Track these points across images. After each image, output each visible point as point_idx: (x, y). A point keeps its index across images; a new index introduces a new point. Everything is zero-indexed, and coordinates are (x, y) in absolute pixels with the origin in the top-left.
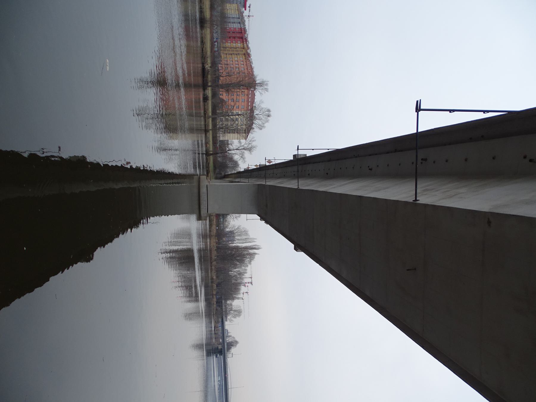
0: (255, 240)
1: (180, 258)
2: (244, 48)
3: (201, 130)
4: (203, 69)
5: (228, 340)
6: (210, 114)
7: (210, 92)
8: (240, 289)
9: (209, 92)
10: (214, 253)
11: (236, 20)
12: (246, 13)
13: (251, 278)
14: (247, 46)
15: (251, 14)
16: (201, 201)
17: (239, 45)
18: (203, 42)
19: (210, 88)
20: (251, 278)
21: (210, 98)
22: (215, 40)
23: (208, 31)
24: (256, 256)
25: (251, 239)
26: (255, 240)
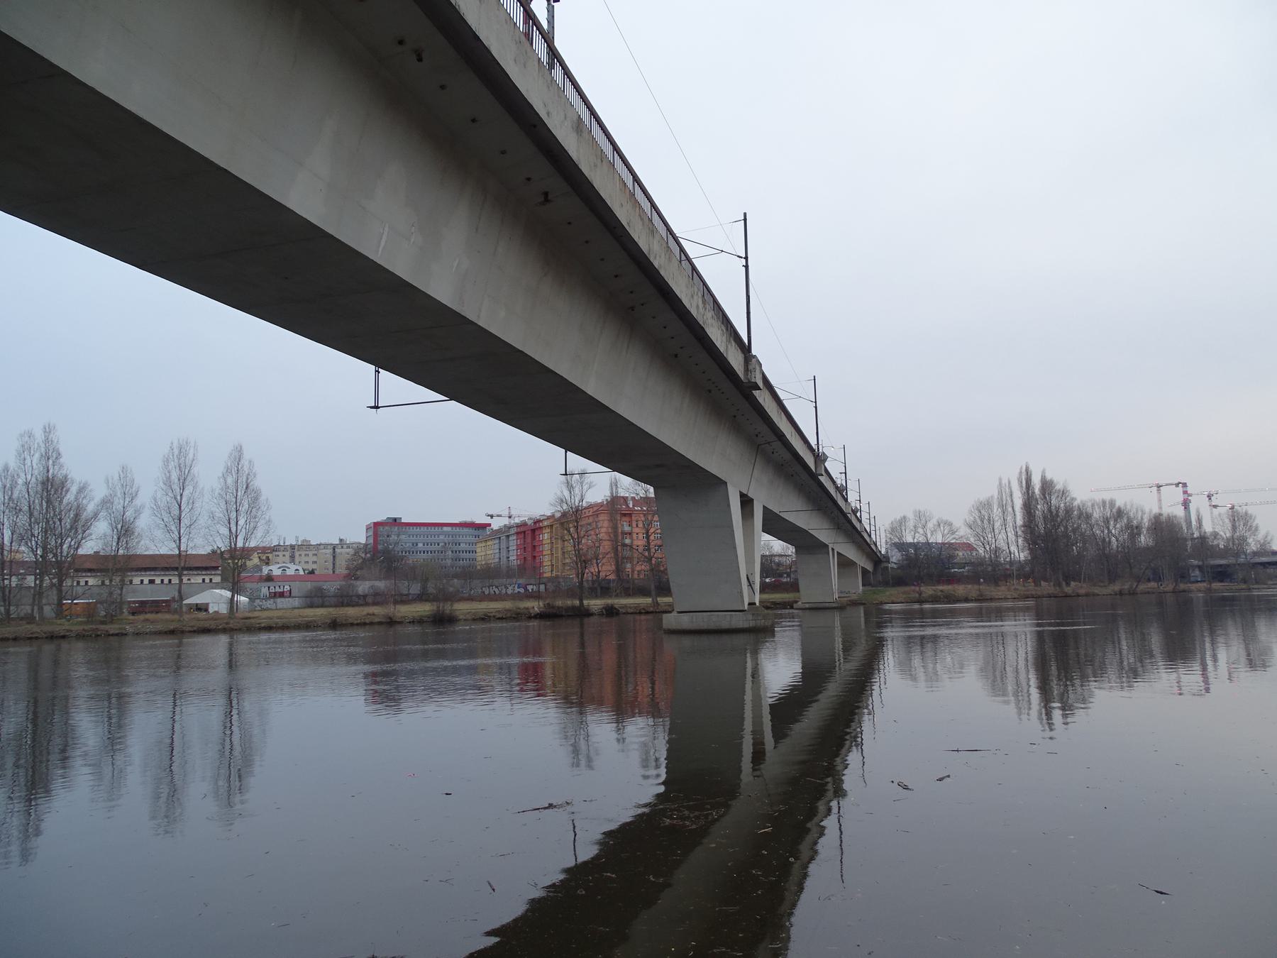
0: (1005, 481)
1: (1066, 673)
2: (551, 526)
3: (231, 644)
4: (541, 616)
5: (1016, 550)
6: (649, 600)
7: (593, 602)
8: (1169, 517)
9: (595, 604)
10: (1046, 587)
11: (504, 545)
12: (496, 524)
13: (1159, 487)
14: (548, 518)
15: (506, 513)
16: (712, 626)
17: (545, 536)
18: (485, 618)
19: (585, 602)
20: (1159, 487)
21: (610, 601)
22: (522, 590)
23: (462, 608)
24: (1049, 476)
25: (1000, 493)
26: (1005, 481)
